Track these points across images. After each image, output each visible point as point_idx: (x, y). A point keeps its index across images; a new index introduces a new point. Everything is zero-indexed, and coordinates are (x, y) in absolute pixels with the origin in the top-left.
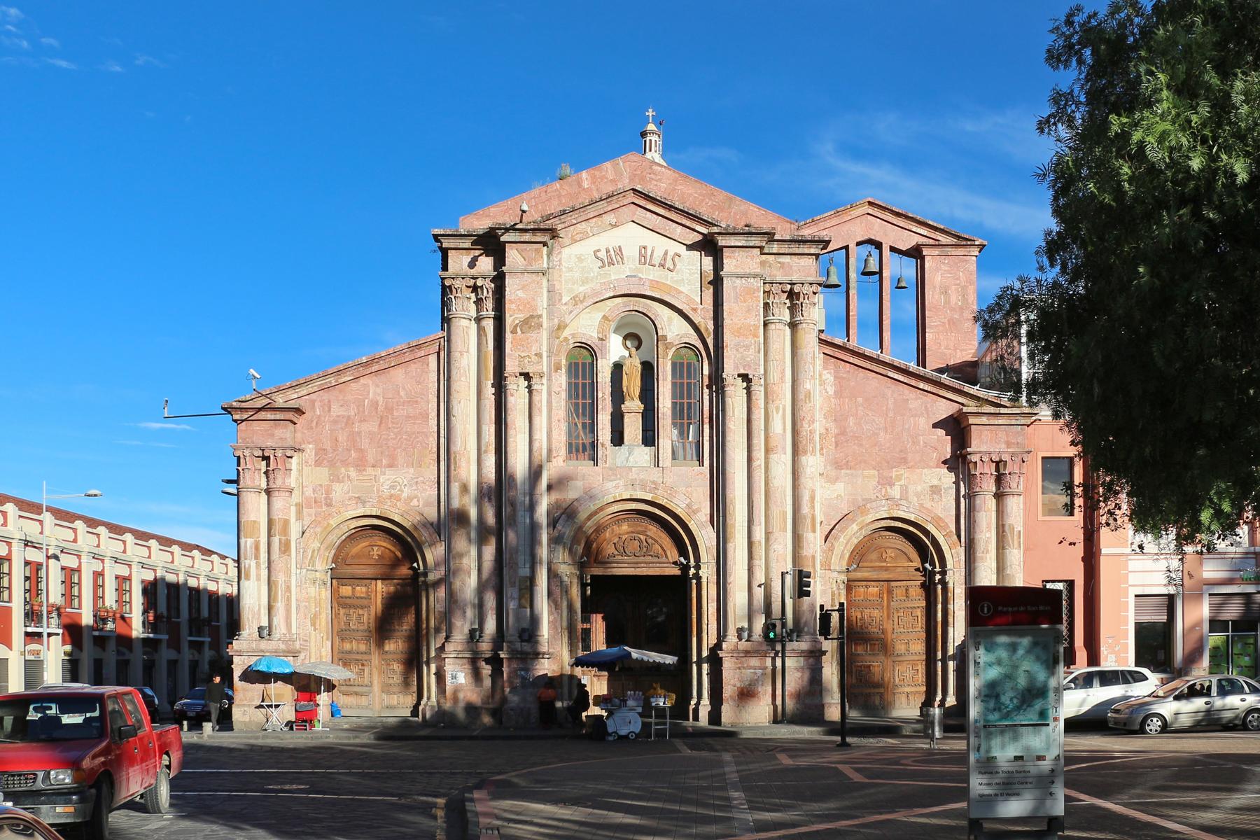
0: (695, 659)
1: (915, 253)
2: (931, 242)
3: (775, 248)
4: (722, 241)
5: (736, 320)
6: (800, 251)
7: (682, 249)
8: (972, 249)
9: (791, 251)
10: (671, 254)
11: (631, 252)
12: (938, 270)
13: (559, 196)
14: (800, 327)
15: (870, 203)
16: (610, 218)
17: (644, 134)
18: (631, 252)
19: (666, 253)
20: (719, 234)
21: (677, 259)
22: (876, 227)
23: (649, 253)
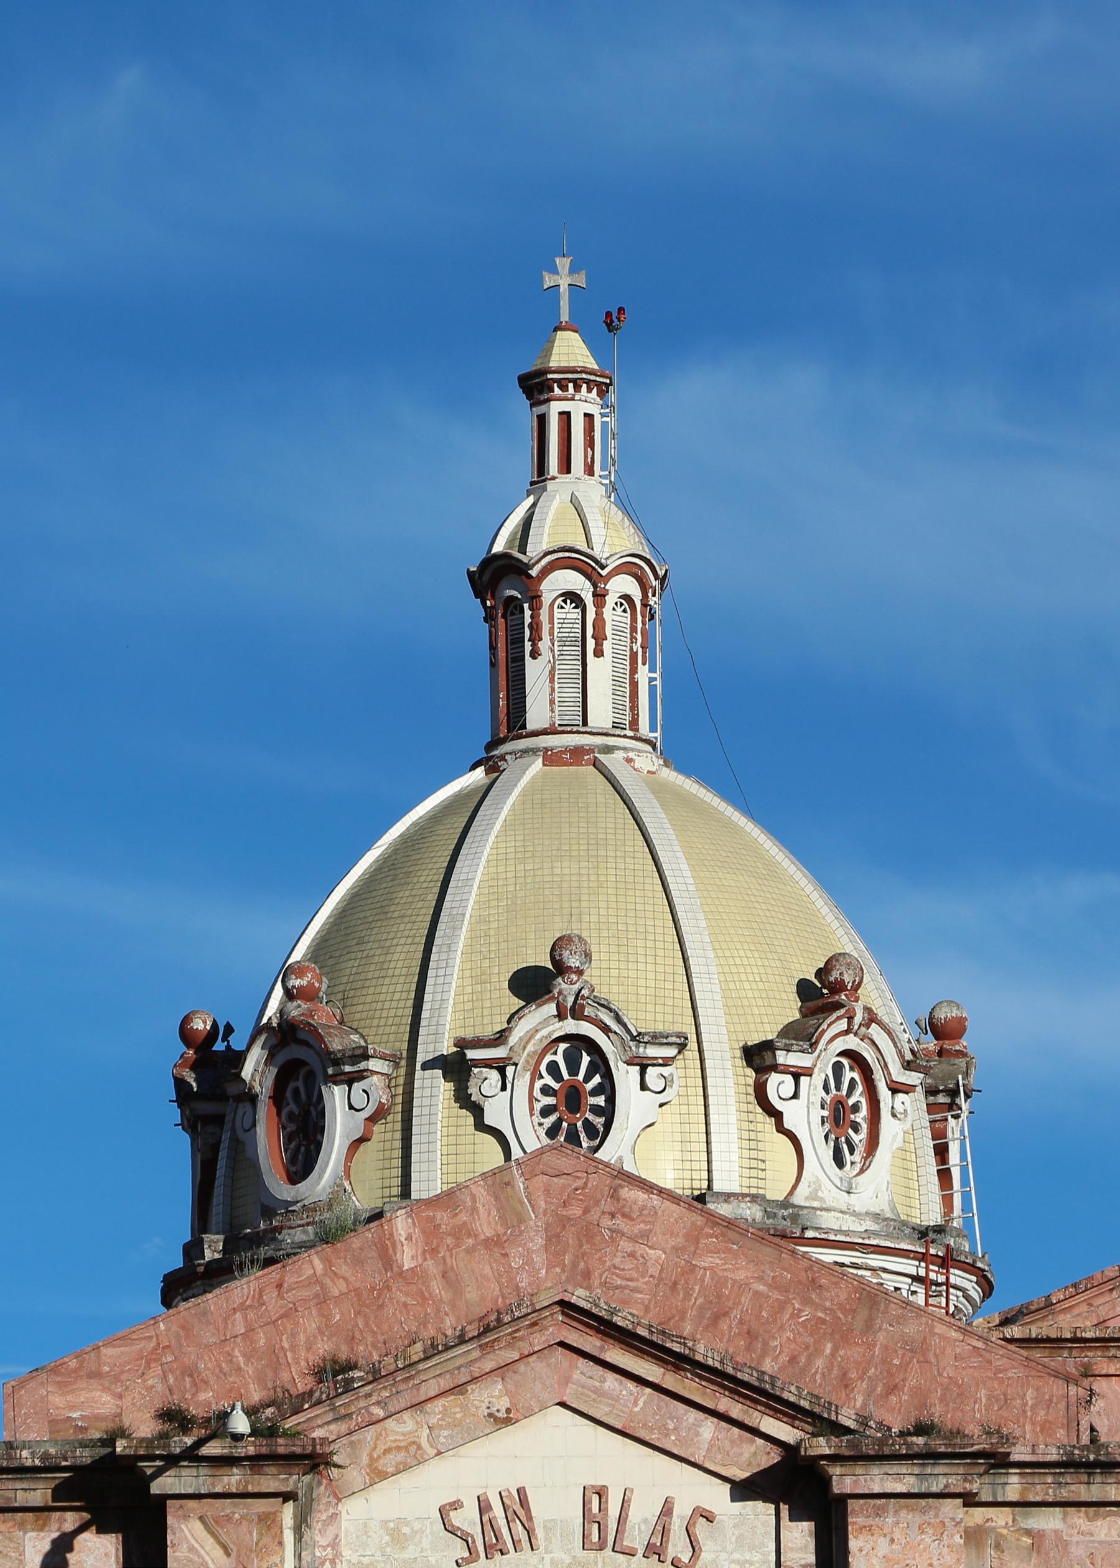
0: (967, 1140)
3: (1013, 1486)
4: (843, 1480)
7: (717, 1497)
9: (1064, 1494)
10: (682, 1511)
11: (557, 1509)
13: (322, 1300)
16: (491, 1396)
17: (536, 386)
18: (557, 1509)
19: (667, 1510)
20: (834, 1458)
21: (701, 1528)
23: (614, 1510)
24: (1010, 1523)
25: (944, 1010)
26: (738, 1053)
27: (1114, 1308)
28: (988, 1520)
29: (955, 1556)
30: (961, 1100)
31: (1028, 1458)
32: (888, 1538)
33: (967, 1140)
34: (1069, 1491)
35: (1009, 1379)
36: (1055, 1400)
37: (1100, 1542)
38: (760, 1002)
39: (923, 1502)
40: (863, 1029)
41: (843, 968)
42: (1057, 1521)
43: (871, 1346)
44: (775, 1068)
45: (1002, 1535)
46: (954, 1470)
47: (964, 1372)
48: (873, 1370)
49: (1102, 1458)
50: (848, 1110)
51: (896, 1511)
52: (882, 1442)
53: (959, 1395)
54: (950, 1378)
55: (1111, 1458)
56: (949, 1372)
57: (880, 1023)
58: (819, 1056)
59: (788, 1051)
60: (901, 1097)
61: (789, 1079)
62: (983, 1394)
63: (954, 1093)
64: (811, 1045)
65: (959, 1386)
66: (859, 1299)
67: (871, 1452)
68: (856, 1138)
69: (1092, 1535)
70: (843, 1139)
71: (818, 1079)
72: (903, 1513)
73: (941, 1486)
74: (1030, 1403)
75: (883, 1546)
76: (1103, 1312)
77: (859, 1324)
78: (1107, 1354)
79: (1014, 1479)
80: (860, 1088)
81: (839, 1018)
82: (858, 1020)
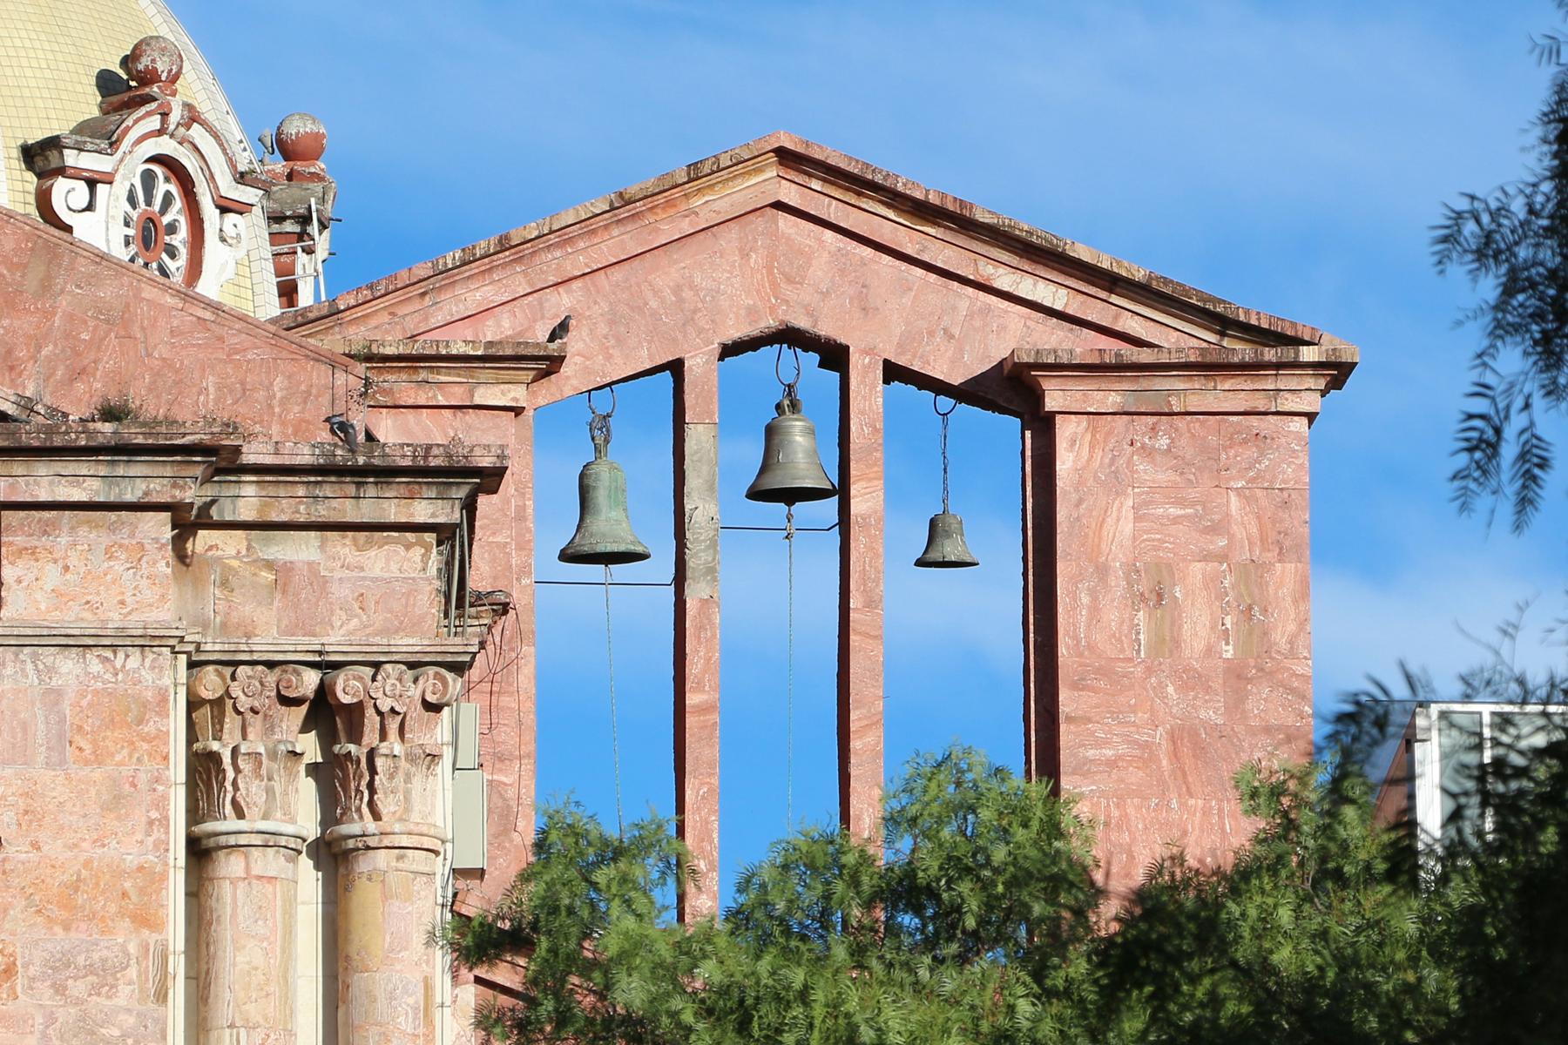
0: (321, 278)
1: (1012, 390)
2: (1083, 345)
3: (247, 500)
5: (54, 849)
6: (366, 511)
8: (1286, 381)
9: (323, 513)
12: (1116, 483)
14: (364, 864)
15: (786, 157)
22: (819, 271)
24: (244, 552)
25: (295, 123)
26: (16, 153)
27: (426, 319)
28: (211, 548)
29: (158, 590)
30: (314, 228)
31: (269, 460)
32: (60, 563)
33: (321, 278)
34: (329, 508)
35: (249, 361)
36: (314, 391)
37: (375, 580)
38: (46, 94)
39: (113, 516)
40: (182, 130)
41: (156, 55)
42: (312, 550)
43: (49, 314)
44: (61, 171)
45: (230, 568)
46: (159, 471)
47: (184, 353)
48: (51, 347)
49: (376, 462)
50: (161, 231)
51: (72, 528)
52: (50, 431)
53: (176, 383)
54: (164, 359)
55: (388, 462)
56: (162, 351)
57: (203, 123)
58: (122, 160)
59: (81, 150)
60: (231, 218)
61: (82, 187)
62: (211, 381)
63: (305, 220)
64: (111, 145)
65: (177, 371)
66: (32, 249)
67: (36, 443)
68: (171, 265)
69: (362, 569)
70: (154, 265)
71: (120, 188)
72: (83, 531)
73: (139, 493)
74: (279, 395)
75: (52, 576)
76: (411, 326)
77: (32, 283)
78: (414, 378)
79: (250, 490)
80: (178, 204)
81: (149, 114)
82: (175, 117)
